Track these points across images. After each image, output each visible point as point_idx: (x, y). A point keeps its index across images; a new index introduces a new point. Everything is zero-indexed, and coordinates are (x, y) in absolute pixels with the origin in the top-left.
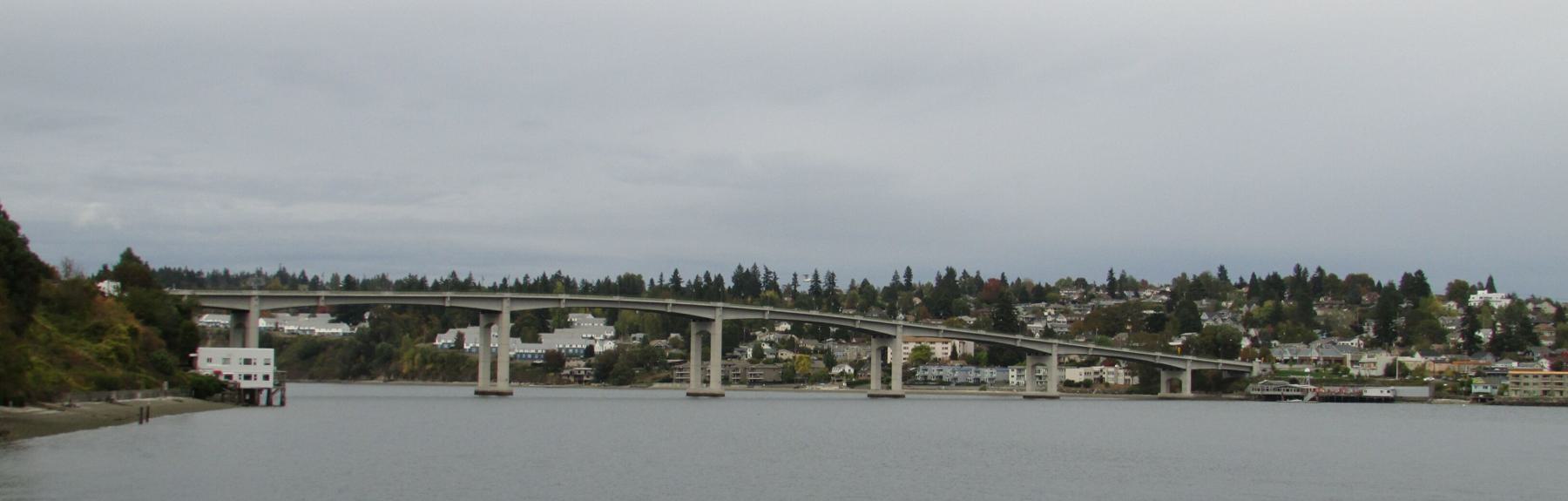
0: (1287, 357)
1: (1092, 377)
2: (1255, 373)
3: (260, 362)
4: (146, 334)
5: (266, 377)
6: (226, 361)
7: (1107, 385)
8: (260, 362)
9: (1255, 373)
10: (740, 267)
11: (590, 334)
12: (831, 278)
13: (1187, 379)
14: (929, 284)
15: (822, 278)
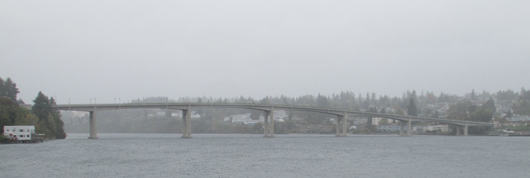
0: (514, 120)
1: (437, 129)
2: (495, 127)
3: (26, 131)
4: (47, 120)
5: (28, 136)
6: (14, 130)
7: (441, 132)
8: (26, 131)
9: (495, 127)
10: (342, 92)
11: (280, 116)
12: (374, 95)
13: (466, 130)
14: (517, 93)
15: (370, 96)
